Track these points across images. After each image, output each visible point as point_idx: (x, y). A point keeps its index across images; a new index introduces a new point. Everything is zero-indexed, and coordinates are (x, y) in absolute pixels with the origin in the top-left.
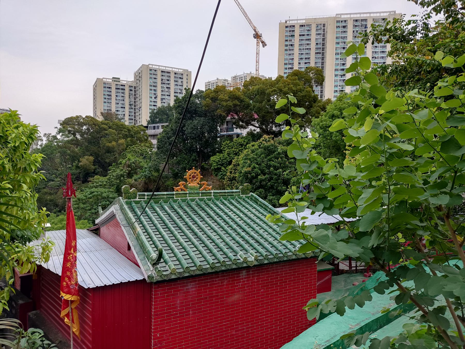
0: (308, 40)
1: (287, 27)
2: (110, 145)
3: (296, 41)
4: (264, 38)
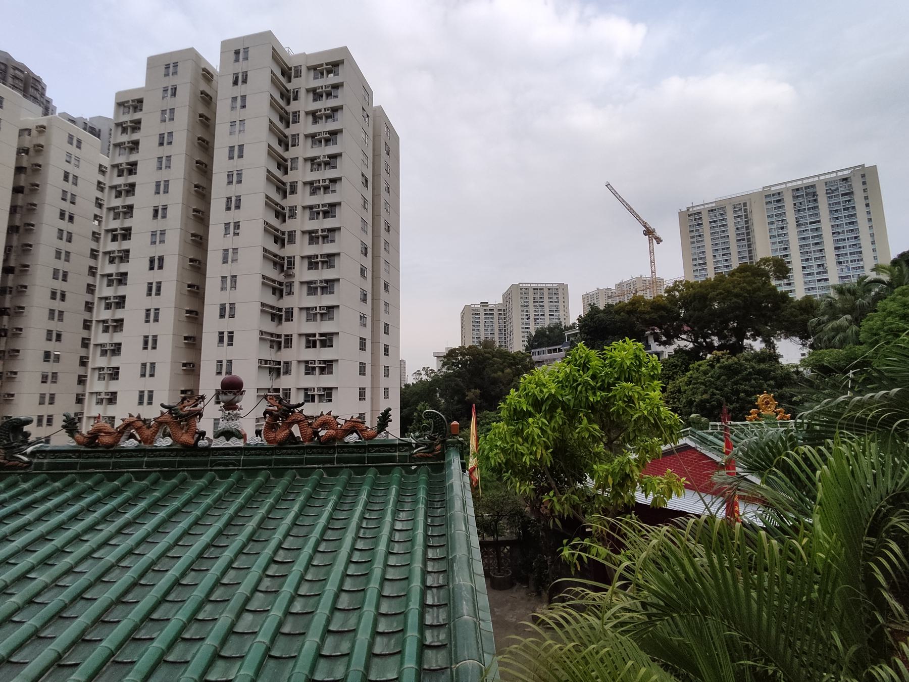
0: (723, 226)
1: (689, 216)
2: (495, 375)
3: (706, 230)
4: (658, 233)
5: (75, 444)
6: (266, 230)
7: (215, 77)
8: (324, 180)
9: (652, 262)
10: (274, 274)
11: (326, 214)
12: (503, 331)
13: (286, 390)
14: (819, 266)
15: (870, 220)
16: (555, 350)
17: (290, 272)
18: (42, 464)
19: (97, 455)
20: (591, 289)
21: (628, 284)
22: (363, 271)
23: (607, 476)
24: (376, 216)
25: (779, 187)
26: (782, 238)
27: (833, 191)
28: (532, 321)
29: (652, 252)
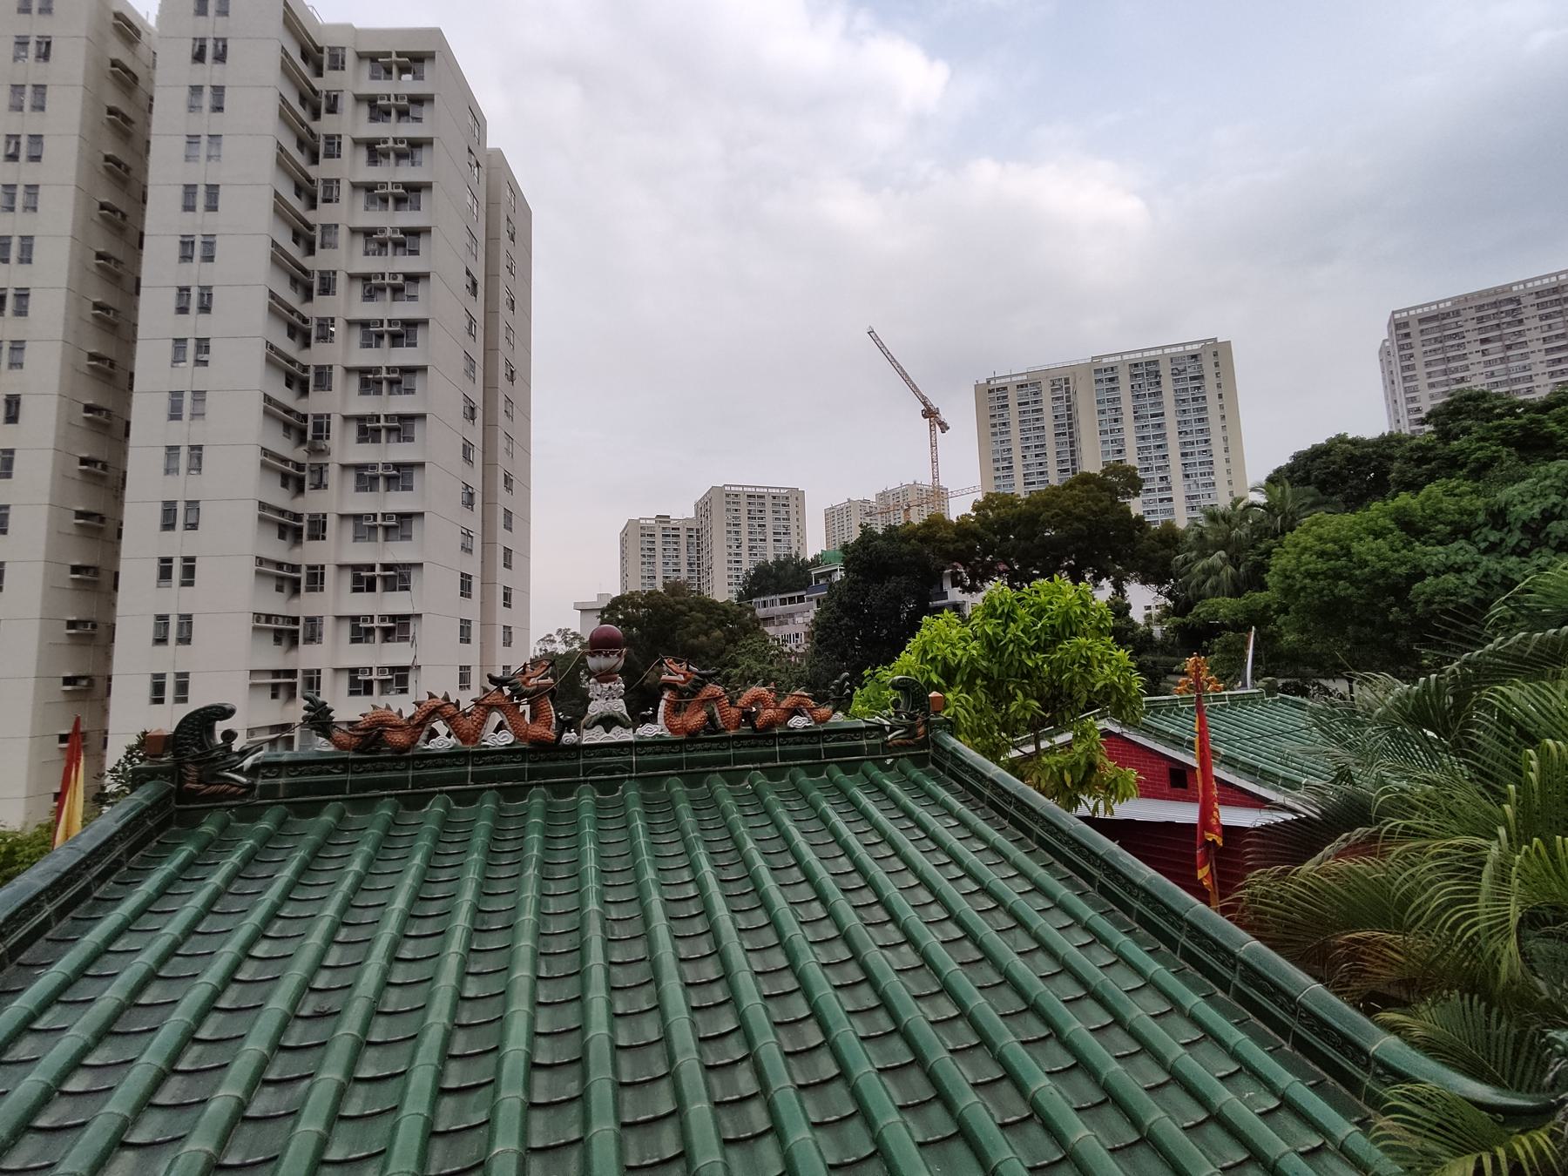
2: (695, 642)
3: (1013, 414)
4: (943, 416)
5: (332, 749)
6: (269, 360)
7: (143, 35)
8: (394, 275)
9: (934, 461)
10: (284, 446)
11: (396, 339)
12: (695, 565)
13: (311, 672)
14: (1162, 479)
16: (792, 600)
17: (321, 444)
18: (277, 786)
19: (379, 765)
20: (839, 500)
21: (896, 494)
22: (467, 449)
23: (1062, 775)
24: (490, 349)
25: (1112, 359)
26: (1116, 436)
27: (1180, 373)
28: (744, 550)
29: (933, 445)
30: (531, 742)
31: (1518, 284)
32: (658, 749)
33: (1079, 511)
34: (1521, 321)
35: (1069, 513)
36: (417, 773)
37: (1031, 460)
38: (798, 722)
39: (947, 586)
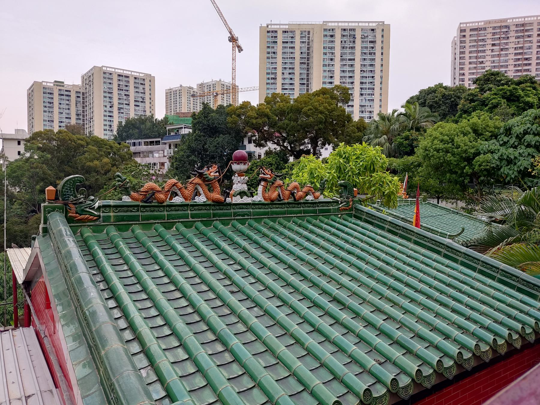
1: (268, 32)
2: (91, 164)
4: (240, 42)
5: (130, 200)
15: (382, 65)
16: (152, 143)
18: (110, 216)
20: (175, 85)
21: (209, 86)
25: (333, 24)
29: (234, 59)
30: (213, 201)
31: (510, 19)
32: (260, 206)
33: (321, 108)
34: (508, 38)
35: (316, 109)
36: (169, 213)
37: (287, 76)
38: (310, 198)
39: (246, 142)
